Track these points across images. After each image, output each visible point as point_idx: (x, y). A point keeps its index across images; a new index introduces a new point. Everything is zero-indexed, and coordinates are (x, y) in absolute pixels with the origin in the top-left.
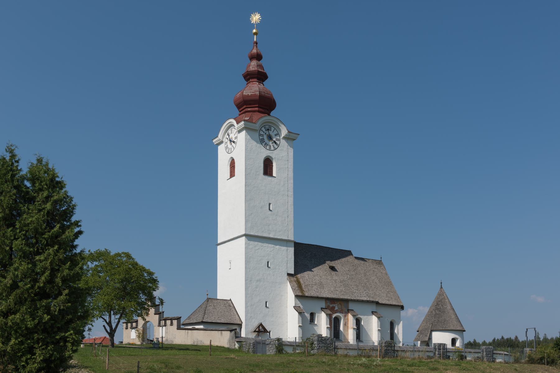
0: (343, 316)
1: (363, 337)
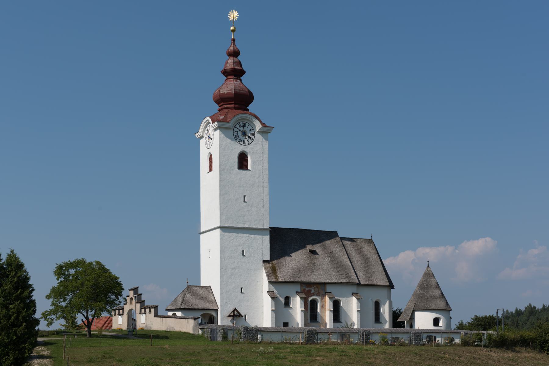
0: (320, 299)
1: (342, 318)
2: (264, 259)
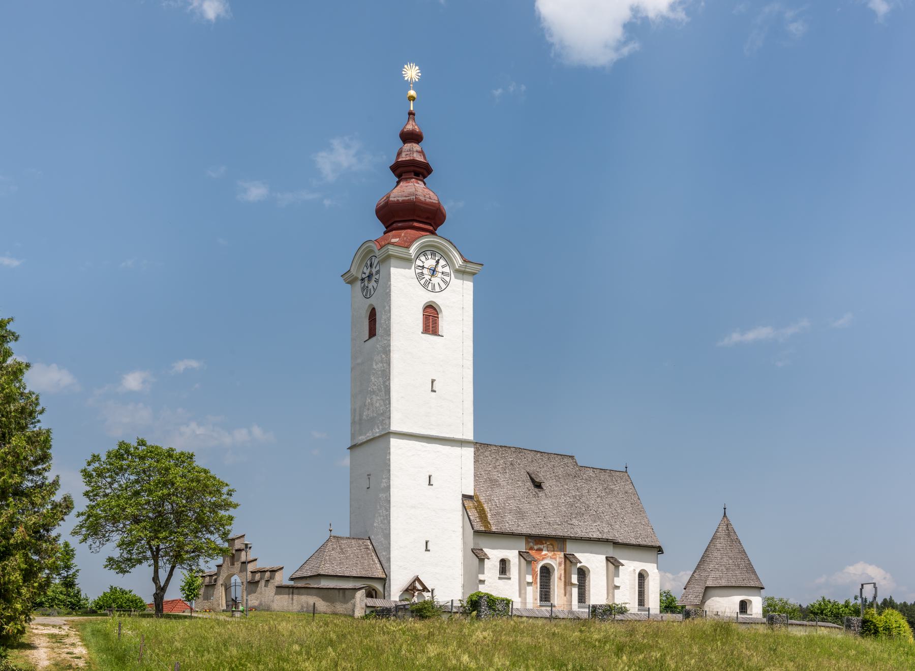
0: (556, 565)
2: (464, 493)
